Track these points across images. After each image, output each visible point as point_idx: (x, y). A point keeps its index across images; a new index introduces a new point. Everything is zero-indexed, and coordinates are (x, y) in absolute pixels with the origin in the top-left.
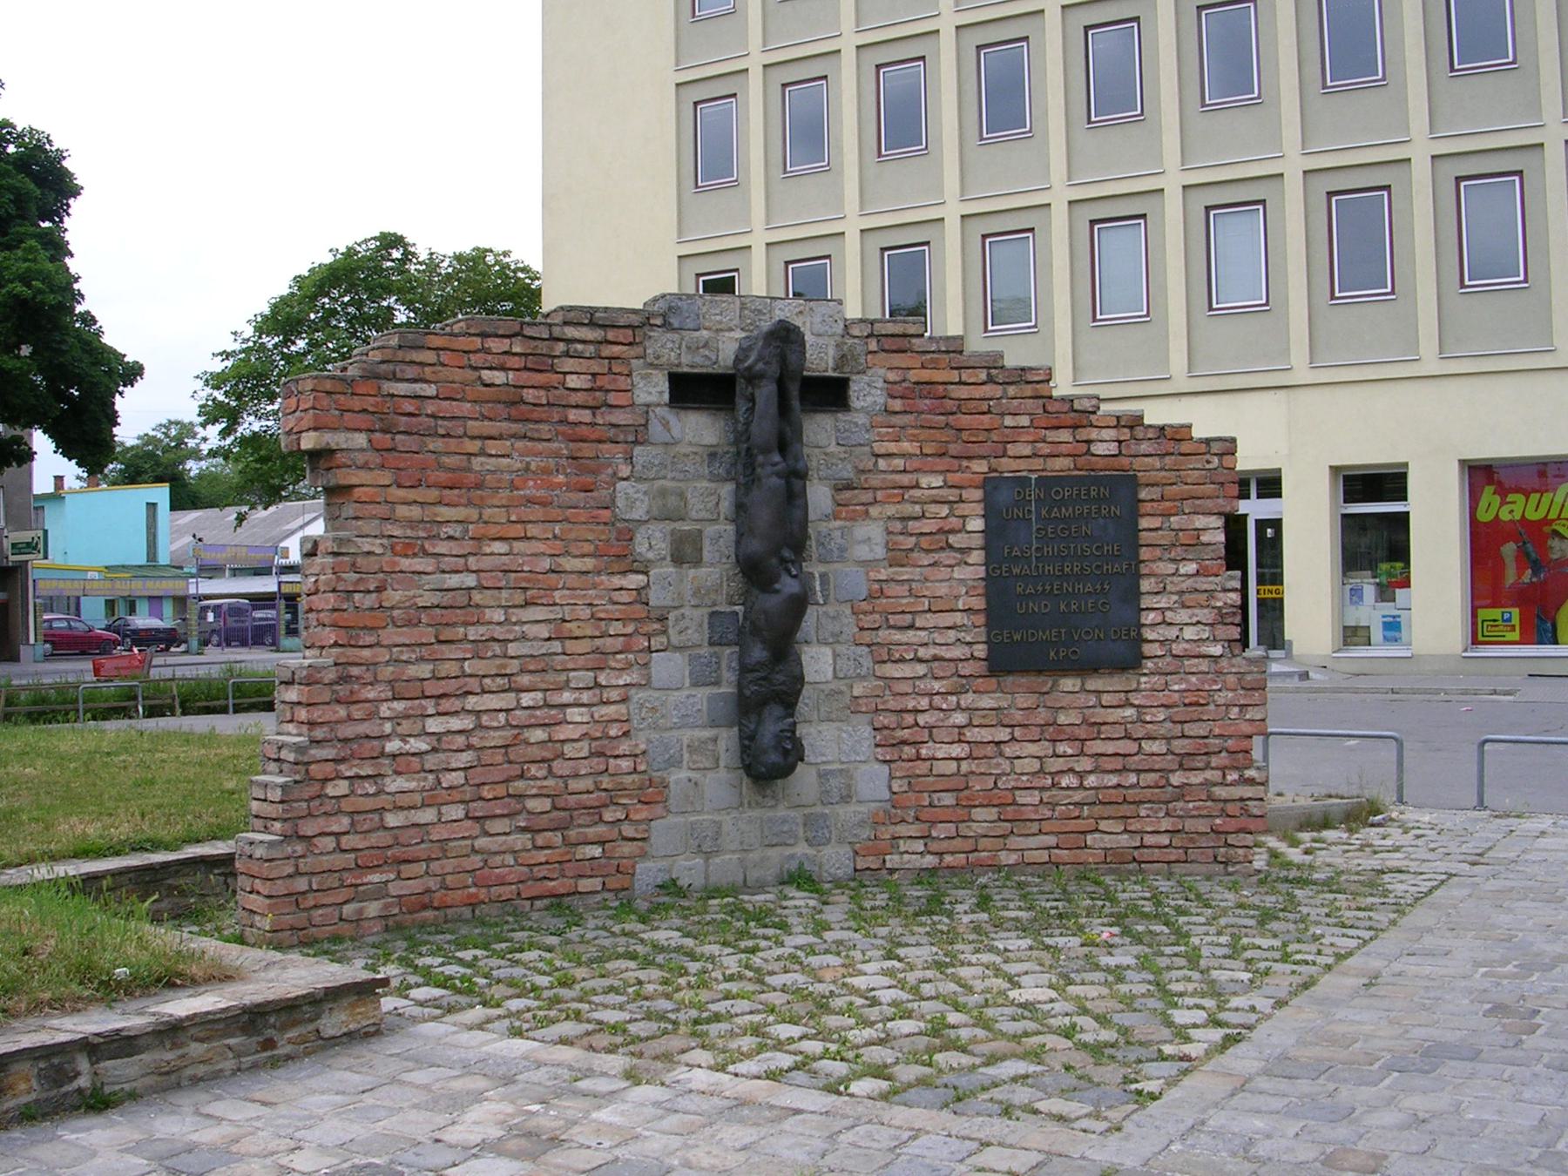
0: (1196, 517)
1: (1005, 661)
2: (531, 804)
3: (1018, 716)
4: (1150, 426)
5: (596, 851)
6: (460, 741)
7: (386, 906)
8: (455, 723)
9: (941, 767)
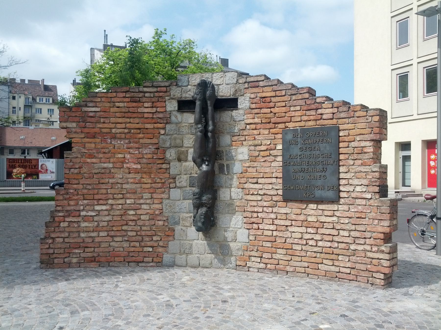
0: (361, 142)
1: (289, 197)
2: (130, 234)
3: (294, 217)
5: (151, 249)
6: (106, 213)
7: (79, 260)
8: (104, 208)
9: (266, 233)
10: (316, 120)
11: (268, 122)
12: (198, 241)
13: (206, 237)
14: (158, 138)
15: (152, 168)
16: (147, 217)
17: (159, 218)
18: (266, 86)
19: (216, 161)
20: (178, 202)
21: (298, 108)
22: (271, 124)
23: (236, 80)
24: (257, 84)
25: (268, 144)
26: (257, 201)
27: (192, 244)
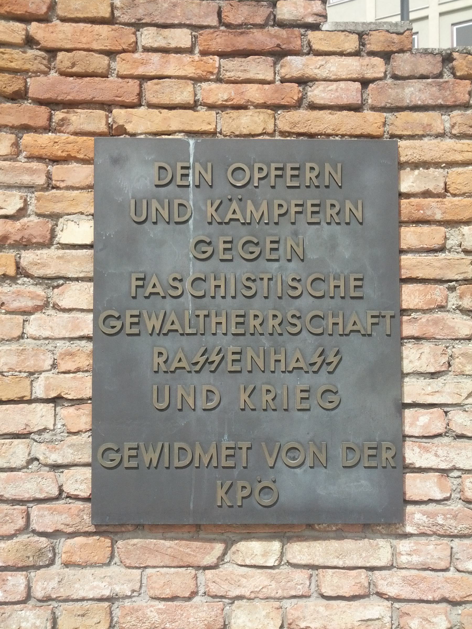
1: (122, 509)
4: (426, 52)
10: (276, 107)
21: (182, 38)
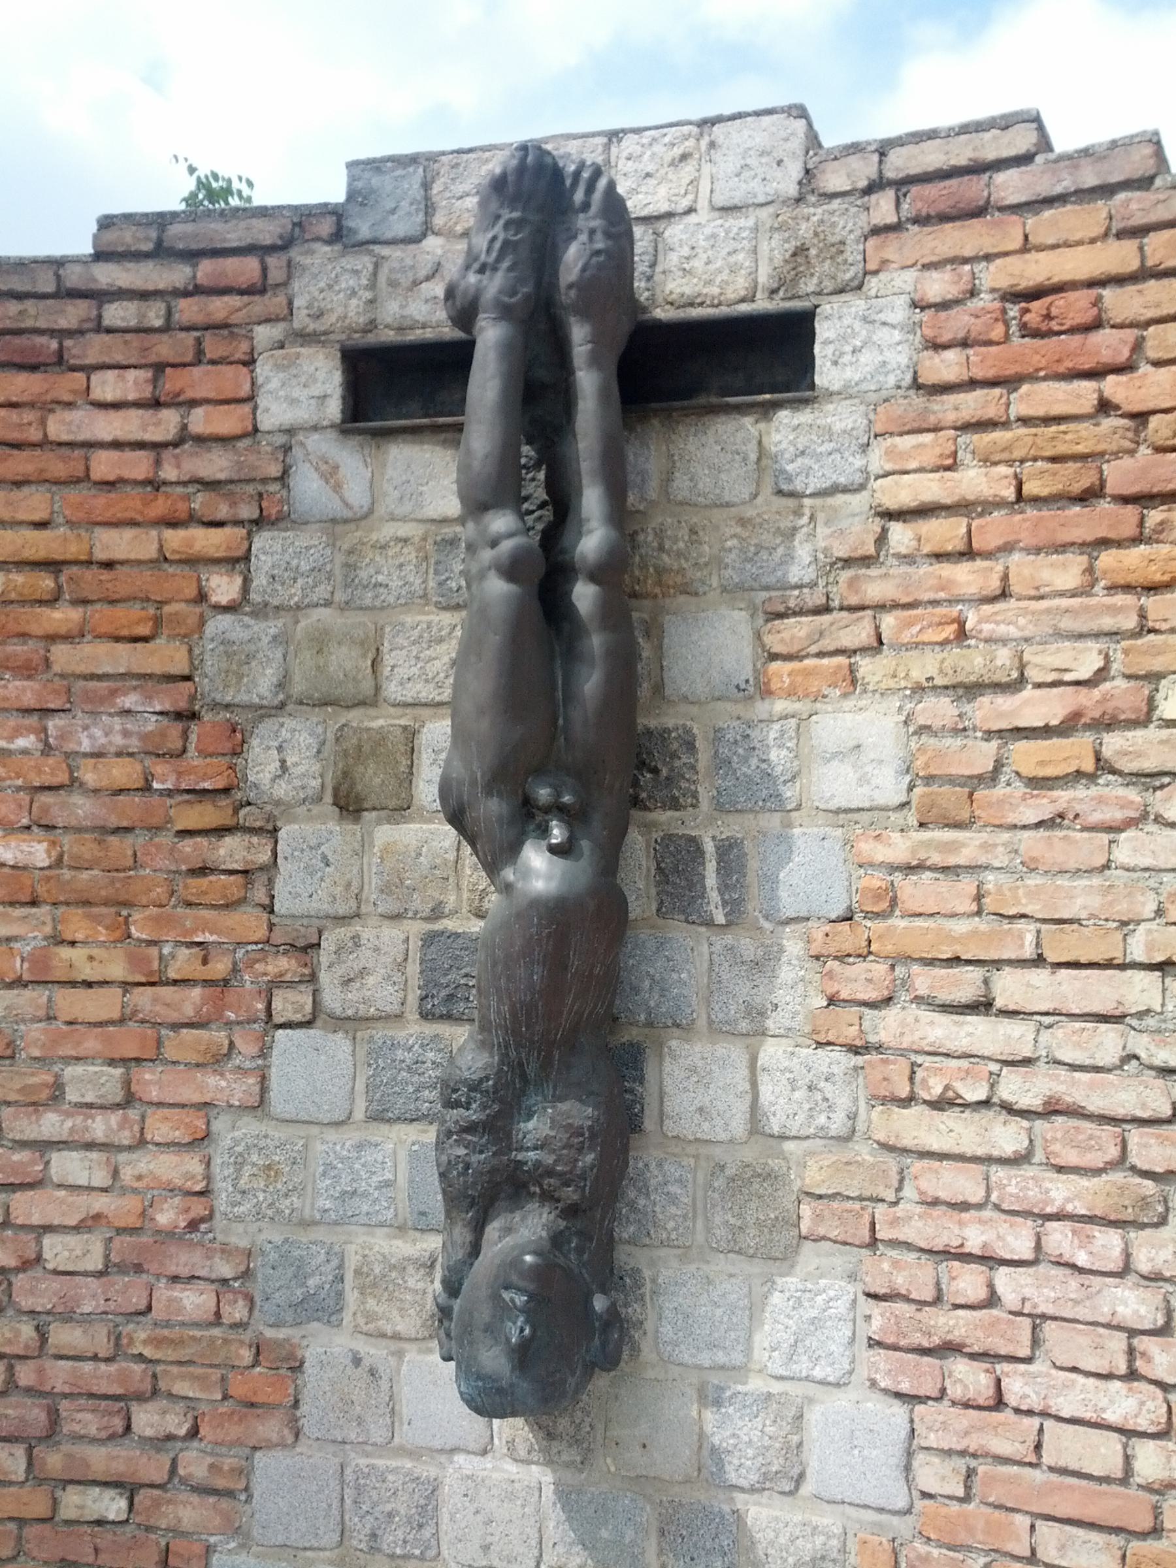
5: (114, 1506)
9: (1065, 1447)
11: (1077, 488)
12: (488, 1462)
13: (550, 1436)
14: (191, 635)
15: (136, 864)
16: (88, 1252)
17: (183, 1261)
18: (1049, 201)
19: (636, 814)
20: (331, 1135)
22: (1105, 505)
23: (795, 171)
24: (972, 189)
25: (1084, 673)
26: (988, 1160)
27: (434, 1488)
